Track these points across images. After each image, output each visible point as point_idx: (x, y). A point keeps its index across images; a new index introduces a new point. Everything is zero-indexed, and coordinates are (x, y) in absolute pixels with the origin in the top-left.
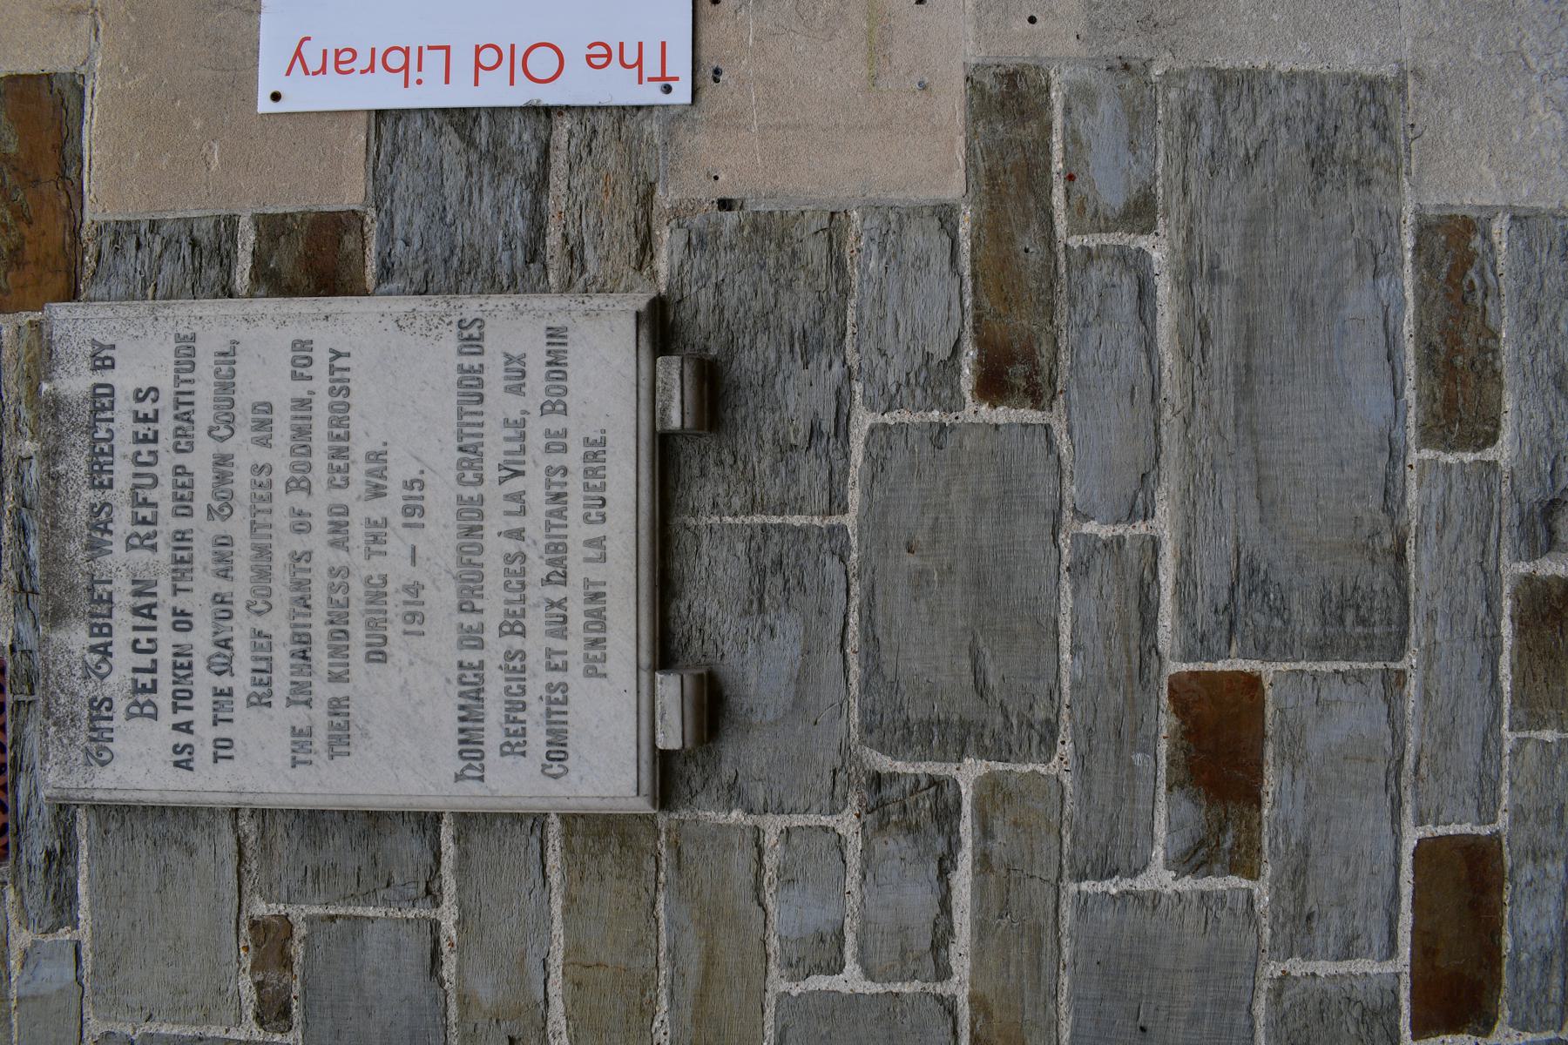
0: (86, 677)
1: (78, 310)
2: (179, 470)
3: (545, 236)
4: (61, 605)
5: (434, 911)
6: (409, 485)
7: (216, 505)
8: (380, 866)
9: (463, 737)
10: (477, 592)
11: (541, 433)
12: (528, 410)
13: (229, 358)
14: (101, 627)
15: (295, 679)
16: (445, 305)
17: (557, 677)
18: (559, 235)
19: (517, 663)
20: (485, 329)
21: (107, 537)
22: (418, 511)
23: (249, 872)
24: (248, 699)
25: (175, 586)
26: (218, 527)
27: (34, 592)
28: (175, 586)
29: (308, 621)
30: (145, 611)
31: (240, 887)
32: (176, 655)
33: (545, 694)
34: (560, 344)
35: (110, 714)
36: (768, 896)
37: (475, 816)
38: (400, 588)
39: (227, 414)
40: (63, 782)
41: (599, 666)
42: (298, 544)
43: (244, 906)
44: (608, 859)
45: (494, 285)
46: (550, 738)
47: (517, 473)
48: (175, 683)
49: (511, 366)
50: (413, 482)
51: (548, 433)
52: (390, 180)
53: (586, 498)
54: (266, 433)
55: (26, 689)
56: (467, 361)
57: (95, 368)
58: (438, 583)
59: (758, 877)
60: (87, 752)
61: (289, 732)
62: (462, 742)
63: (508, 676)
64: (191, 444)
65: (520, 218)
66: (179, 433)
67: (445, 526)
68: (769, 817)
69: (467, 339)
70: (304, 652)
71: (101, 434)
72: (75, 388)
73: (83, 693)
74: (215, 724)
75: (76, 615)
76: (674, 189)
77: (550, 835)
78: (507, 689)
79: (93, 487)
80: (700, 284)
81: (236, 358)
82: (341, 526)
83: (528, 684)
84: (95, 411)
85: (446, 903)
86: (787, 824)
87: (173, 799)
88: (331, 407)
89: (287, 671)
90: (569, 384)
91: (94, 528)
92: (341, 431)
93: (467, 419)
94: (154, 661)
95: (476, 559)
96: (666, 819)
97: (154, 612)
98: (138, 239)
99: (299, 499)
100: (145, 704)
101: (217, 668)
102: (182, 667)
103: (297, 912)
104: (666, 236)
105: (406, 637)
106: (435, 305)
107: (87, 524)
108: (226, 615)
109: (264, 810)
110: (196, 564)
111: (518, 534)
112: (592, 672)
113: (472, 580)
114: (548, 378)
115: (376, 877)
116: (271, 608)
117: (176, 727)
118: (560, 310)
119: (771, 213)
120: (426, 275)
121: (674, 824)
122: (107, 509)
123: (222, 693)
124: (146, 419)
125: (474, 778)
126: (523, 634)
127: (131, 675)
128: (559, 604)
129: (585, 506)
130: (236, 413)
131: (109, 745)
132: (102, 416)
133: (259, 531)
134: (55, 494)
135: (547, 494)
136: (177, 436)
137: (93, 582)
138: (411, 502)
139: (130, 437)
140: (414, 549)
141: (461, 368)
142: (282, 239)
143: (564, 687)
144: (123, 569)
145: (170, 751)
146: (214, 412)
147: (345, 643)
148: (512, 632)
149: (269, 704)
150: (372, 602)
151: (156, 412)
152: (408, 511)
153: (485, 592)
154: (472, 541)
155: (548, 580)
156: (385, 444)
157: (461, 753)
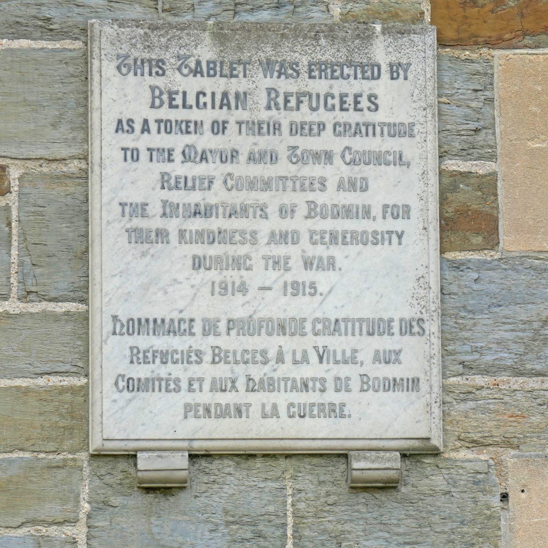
0: (179, 57)
1: (431, 52)
2: (322, 126)
3: (482, 374)
4: (229, 41)
5: (16, 297)
6: (313, 286)
7: (299, 152)
8: (47, 259)
9: (143, 321)
10: (241, 332)
11: (348, 374)
12: (363, 366)
13: (398, 161)
14: (214, 69)
15: (181, 206)
16: (434, 309)
17: (184, 385)
18: (483, 384)
19: (194, 358)
20: (417, 336)
21: (276, 74)
22: (295, 291)
23: (41, 166)
24: (166, 173)
25: (243, 123)
26: (283, 153)
27: (236, 13)
28: (243, 123)
29: (221, 216)
30: (225, 101)
31: (30, 159)
32: (196, 123)
33: (173, 377)
34: (408, 387)
35: (154, 74)
36: (28, 529)
37: (87, 327)
38: (244, 279)
39: (360, 160)
40: (105, 39)
41: (192, 413)
42: (272, 210)
43: (16, 162)
44: (55, 418)
45: (445, 341)
46: (143, 380)
47: (321, 358)
48: (177, 121)
49: (393, 354)
50: (315, 288)
51: (348, 379)
52: (520, 268)
53: (305, 405)
54: (347, 187)
55: (167, 7)
56: (396, 326)
57: (391, 65)
58: (247, 305)
59: (43, 522)
60: (127, 57)
61: (143, 201)
62: (139, 320)
63: (185, 352)
64: (340, 135)
65: (494, 357)
66: (347, 126)
67: (285, 310)
68: (85, 530)
69: (411, 325)
70: (200, 213)
71: (346, 71)
72: (378, 51)
73: (168, 56)
74: (148, 149)
75: (221, 51)
76: (515, 463)
77: (71, 378)
78: (176, 351)
79: (310, 64)
80: (450, 480)
81: (398, 166)
82: (285, 239)
83: (180, 366)
84: (362, 66)
85: (22, 305)
86: (80, 542)
87: (95, 116)
88: (365, 232)
89: (187, 200)
90: (381, 394)
91: (282, 66)
92: (348, 239)
93: (357, 325)
94: (191, 107)
95: (263, 331)
96: (84, 458)
97: (225, 108)
98: (481, 90)
99: (303, 210)
100: (161, 100)
101: (187, 151)
102: (187, 127)
103: (12, 199)
104: (482, 457)
105: (210, 284)
106: (434, 302)
107: (284, 60)
108: (224, 159)
109: (87, 178)
110: (258, 138)
111: (280, 359)
112: (188, 408)
113: (249, 328)
114: (385, 379)
115: (39, 256)
116: (229, 190)
117: (146, 121)
118: (431, 387)
119: (500, 529)
120: (455, 294)
121: (79, 463)
122: (295, 74)
123: (170, 155)
124: (357, 103)
125: (115, 328)
126: (213, 362)
127: (181, 90)
128: (234, 387)
129: (299, 404)
130: (360, 166)
131: (132, 73)
132: (359, 71)
133: (281, 182)
134: (305, 37)
135: (307, 379)
136: (345, 125)
137: (245, 64)
138: (301, 287)
139: (344, 91)
140: (270, 289)
141: (391, 320)
142: (479, 193)
143: (178, 390)
144: (254, 86)
145: (129, 117)
146: (361, 150)
147: (206, 241)
148: (214, 355)
149: (163, 188)
150: (233, 260)
151: (361, 110)
152: (295, 285)
153: (241, 337)
154: (276, 328)
155: (249, 379)
156: (340, 269)
157: (132, 320)
